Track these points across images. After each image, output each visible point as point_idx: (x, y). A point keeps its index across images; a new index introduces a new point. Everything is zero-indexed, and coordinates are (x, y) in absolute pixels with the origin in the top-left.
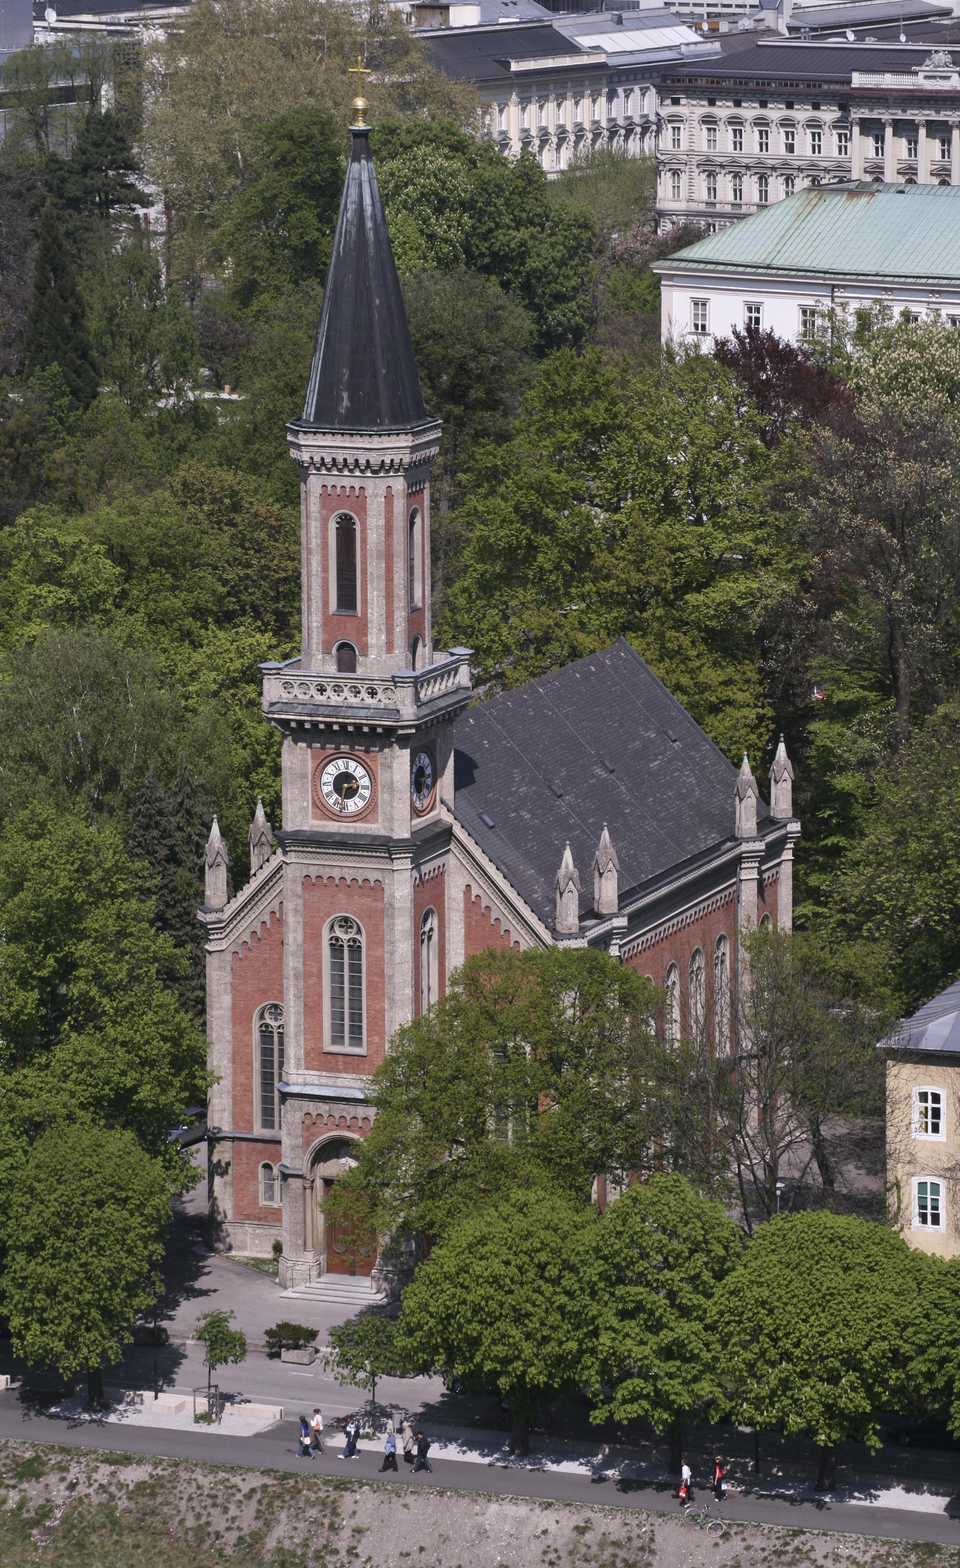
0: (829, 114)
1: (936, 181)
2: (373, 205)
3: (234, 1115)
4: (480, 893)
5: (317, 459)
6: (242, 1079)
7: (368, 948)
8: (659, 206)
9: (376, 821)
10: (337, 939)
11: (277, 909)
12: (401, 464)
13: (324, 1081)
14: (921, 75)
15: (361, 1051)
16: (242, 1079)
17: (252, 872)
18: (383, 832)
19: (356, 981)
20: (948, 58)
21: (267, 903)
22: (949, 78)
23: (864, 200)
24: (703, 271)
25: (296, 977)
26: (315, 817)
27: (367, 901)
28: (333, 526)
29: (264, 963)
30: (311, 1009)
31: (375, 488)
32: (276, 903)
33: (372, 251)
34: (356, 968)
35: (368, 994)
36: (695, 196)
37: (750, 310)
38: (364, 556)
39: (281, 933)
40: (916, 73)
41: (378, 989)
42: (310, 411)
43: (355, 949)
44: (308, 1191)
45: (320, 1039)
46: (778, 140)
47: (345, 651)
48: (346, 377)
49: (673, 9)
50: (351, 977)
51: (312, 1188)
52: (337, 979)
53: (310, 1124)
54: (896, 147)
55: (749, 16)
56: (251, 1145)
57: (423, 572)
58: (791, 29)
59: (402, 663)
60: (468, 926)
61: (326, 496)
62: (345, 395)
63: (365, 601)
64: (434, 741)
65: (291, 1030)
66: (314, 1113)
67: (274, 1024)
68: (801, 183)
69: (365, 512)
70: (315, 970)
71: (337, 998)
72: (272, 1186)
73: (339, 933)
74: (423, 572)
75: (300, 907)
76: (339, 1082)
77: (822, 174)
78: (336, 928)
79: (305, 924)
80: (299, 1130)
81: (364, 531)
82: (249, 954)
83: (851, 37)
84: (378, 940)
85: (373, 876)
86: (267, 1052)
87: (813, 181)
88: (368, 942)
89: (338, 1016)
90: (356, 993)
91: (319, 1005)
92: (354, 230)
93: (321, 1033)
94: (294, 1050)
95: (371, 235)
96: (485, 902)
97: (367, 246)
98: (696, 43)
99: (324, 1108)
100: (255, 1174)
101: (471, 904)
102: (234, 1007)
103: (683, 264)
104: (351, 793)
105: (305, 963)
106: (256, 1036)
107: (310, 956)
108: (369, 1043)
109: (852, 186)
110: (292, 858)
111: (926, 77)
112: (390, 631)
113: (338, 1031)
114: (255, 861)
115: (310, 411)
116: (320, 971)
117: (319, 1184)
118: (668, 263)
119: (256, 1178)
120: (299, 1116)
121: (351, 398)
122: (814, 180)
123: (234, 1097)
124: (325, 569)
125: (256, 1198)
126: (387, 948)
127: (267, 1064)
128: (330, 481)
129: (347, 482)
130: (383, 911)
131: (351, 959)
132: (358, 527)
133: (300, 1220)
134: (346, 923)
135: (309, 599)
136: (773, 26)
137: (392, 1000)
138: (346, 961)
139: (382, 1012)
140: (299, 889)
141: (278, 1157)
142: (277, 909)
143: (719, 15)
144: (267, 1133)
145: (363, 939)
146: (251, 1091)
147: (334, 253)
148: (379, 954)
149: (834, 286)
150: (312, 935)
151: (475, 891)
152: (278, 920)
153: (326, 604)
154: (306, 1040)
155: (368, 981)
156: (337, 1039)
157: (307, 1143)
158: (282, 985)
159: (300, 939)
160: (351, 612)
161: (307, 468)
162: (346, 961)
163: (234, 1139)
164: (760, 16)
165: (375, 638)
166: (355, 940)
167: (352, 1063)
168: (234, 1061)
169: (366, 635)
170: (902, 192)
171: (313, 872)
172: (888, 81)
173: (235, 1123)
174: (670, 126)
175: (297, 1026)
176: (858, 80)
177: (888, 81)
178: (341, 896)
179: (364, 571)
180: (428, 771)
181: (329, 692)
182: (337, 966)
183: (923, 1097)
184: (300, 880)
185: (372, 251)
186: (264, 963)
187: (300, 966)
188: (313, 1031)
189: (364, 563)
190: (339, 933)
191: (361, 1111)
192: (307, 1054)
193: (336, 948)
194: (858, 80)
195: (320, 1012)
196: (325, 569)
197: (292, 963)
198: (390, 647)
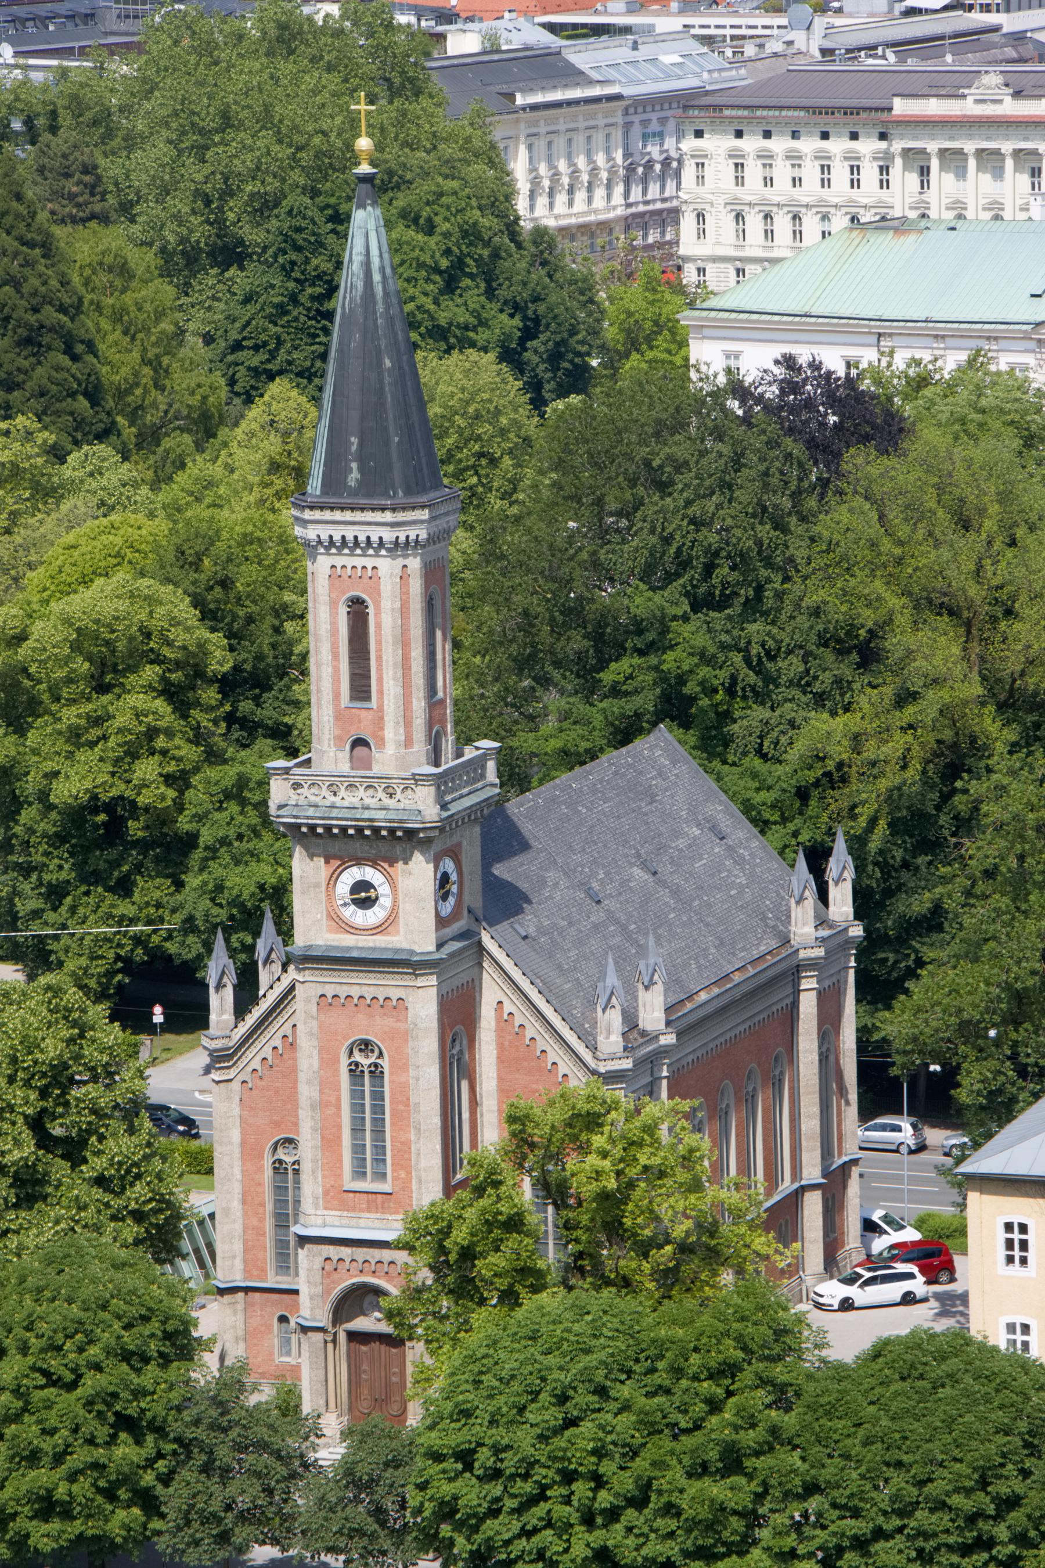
0: (868, 146)
1: (987, 215)
2: (381, 256)
3: (245, 1262)
4: (513, 1010)
5: (324, 537)
6: (254, 1222)
7: (391, 1074)
8: (682, 251)
9: (398, 932)
10: (357, 1064)
11: (289, 1033)
12: (417, 541)
13: (345, 1221)
14: (970, 99)
15: (386, 1187)
16: (254, 1222)
17: (261, 993)
18: (405, 945)
19: (378, 1109)
20: (999, 79)
21: (278, 1028)
22: (1000, 101)
23: (912, 238)
24: (735, 320)
25: (313, 1107)
26: (330, 930)
27: (389, 1022)
28: (343, 611)
29: (277, 1093)
30: (330, 1143)
31: (387, 567)
32: (288, 1026)
33: (380, 307)
34: (378, 1096)
35: (392, 1124)
36: (721, 239)
37: (728, 357)
38: (379, 643)
39: (295, 1059)
40: (964, 96)
41: (402, 1118)
42: (315, 485)
43: (377, 1073)
44: (330, 1346)
45: (340, 1176)
46: (811, 173)
47: (360, 750)
48: (354, 448)
49: (693, 31)
50: (373, 1106)
51: (334, 1342)
52: (358, 1108)
53: (330, 1268)
54: (942, 181)
55: (778, 38)
56: (266, 1295)
57: (406, 660)
58: (824, 52)
59: (423, 759)
60: (501, 1047)
61: (335, 575)
62: (354, 465)
63: (381, 692)
64: (459, 845)
65: (306, 1167)
66: (335, 1258)
67: (289, 1159)
68: (839, 222)
69: (379, 593)
70: (333, 1099)
71: (357, 1130)
72: (288, 1341)
73: (358, 1057)
74: (406, 660)
75: (315, 1030)
76: (362, 1223)
77: (862, 211)
78: (356, 1052)
79: (321, 1049)
80: (318, 1278)
81: (378, 614)
82: (260, 1083)
83: (892, 58)
84: (402, 1066)
85: (394, 994)
86: (280, 1190)
87: (852, 219)
88: (391, 1067)
89: (358, 1149)
90: (379, 1123)
91: (339, 1138)
92: (360, 285)
93: (341, 1168)
94: (311, 1187)
95: (379, 290)
96: (518, 1020)
97: (374, 303)
98: (720, 70)
99: (346, 1252)
100: (269, 1327)
101: (504, 1022)
102: (243, 1143)
103: (713, 314)
104: (366, 903)
105: (321, 1092)
106: (268, 1172)
107: (327, 1084)
108: (394, 1179)
109: (895, 223)
110: (307, 976)
111: (978, 101)
112: (408, 724)
113: (359, 1163)
114: (264, 977)
115: (315, 485)
116: (339, 1099)
117: (342, 1337)
118: (696, 313)
119: (271, 1331)
120: (318, 1262)
121: (361, 469)
122: (854, 219)
123: (245, 1242)
124: (336, 656)
125: (272, 1354)
126: (412, 1073)
127: (280, 1202)
128: (339, 561)
129: (359, 562)
130: (407, 1032)
131: (372, 1085)
132: (371, 610)
133: (322, 1377)
134: (366, 1046)
135: (318, 691)
136: (804, 49)
137: (418, 1130)
138: (367, 1088)
139: (407, 1144)
140: (314, 1009)
141: (296, 1307)
142: (289, 1033)
143: (743, 37)
144: (284, 1282)
145: (385, 1063)
146: (264, 1234)
147: (339, 310)
148: (403, 1079)
149: (880, 335)
150: (328, 1062)
151: (508, 1008)
152: (291, 1044)
153: (337, 696)
154: (324, 1177)
155: (392, 1110)
156: (360, 1173)
157: (327, 1292)
158: (297, 1116)
159: (316, 1064)
160: (366, 705)
161: (315, 548)
162: (367, 1088)
163: (247, 1290)
164: (788, 38)
165: (392, 733)
166: (376, 1065)
167: (379, 1201)
168: (244, 1202)
169: (382, 729)
170: (953, 229)
171: (330, 990)
172: (933, 107)
173: (246, 1271)
174: (693, 162)
175: (314, 1161)
176: (901, 107)
177: (933, 107)
178: (360, 1016)
179: (379, 658)
180: (454, 877)
181: (342, 792)
182: (357, 1095)
183: (1009, 1227)
184: (315, 1000)
185: (380, 307)
186: (277, 1093)
187: (316, 1095)
188: (333, 1168)
189: (379, 650)
190: (358, 1057)
191: (386, 1255)
192: (326, 1193)
193: (355, 1072)
194: (901, 107)
195: (340, 1145)
196: (126, 34)
197: (307, 1092)
198: (408, 742)
